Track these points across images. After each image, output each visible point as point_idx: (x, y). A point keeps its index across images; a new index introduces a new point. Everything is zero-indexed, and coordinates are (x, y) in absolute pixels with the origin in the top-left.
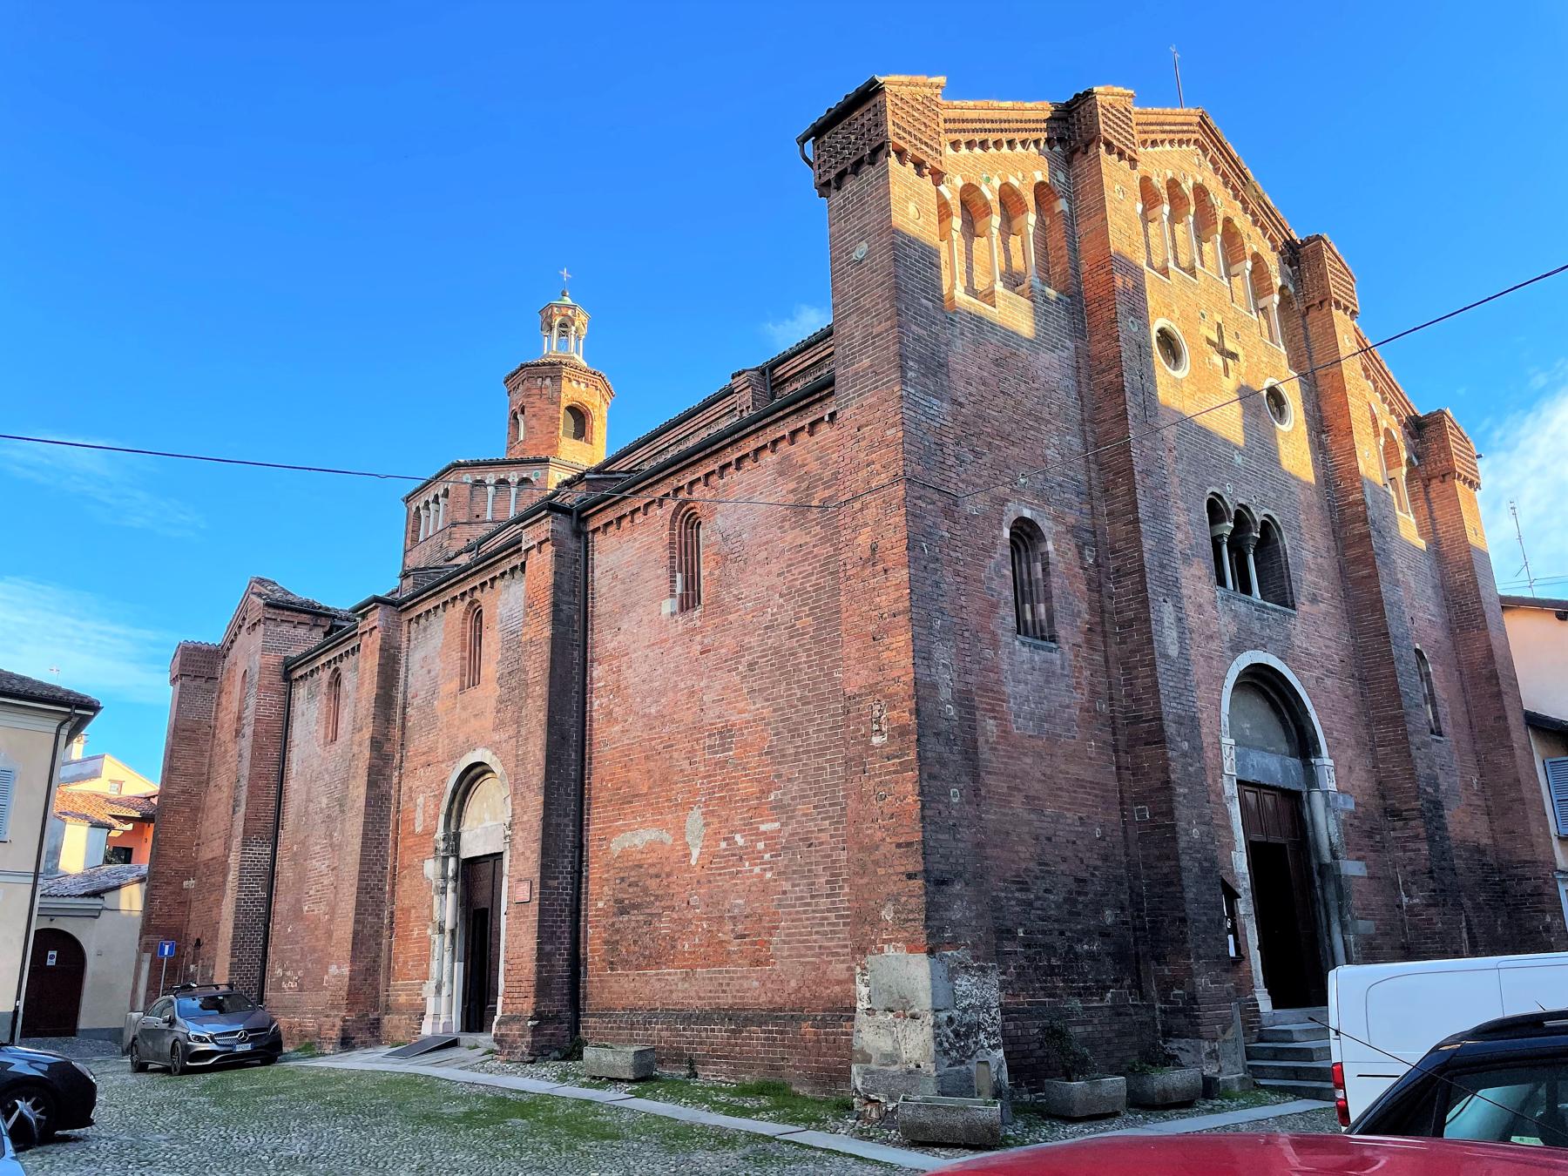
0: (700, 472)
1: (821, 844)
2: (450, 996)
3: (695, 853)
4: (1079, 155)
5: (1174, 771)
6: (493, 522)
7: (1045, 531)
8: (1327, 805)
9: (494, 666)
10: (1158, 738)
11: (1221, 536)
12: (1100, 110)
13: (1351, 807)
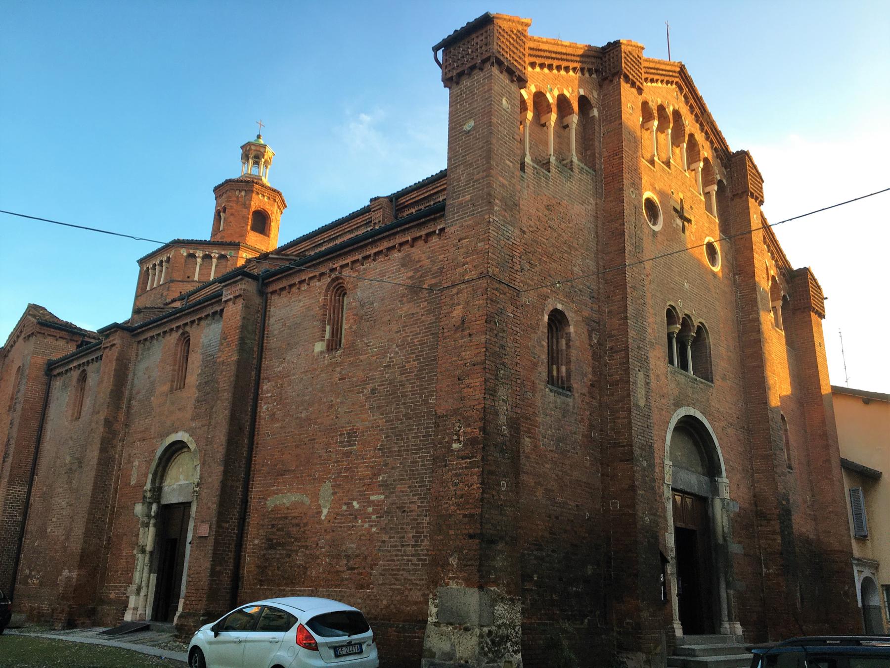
0: (349, 260)
1: (411, 511)
2: (146, 596)
3: (325, 512)
4: (607, 82)
5: (637, 480)
6: (199, 282)
7: (569, 319)
8: (723, 507)
9: (195, 377)
10: (629, 458)
11: (673, 333)
12: (623, 55)
13: (737, 510)
